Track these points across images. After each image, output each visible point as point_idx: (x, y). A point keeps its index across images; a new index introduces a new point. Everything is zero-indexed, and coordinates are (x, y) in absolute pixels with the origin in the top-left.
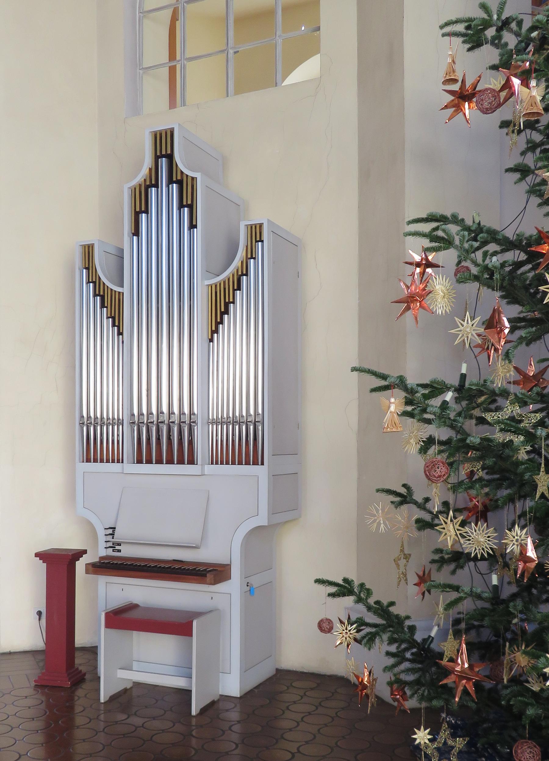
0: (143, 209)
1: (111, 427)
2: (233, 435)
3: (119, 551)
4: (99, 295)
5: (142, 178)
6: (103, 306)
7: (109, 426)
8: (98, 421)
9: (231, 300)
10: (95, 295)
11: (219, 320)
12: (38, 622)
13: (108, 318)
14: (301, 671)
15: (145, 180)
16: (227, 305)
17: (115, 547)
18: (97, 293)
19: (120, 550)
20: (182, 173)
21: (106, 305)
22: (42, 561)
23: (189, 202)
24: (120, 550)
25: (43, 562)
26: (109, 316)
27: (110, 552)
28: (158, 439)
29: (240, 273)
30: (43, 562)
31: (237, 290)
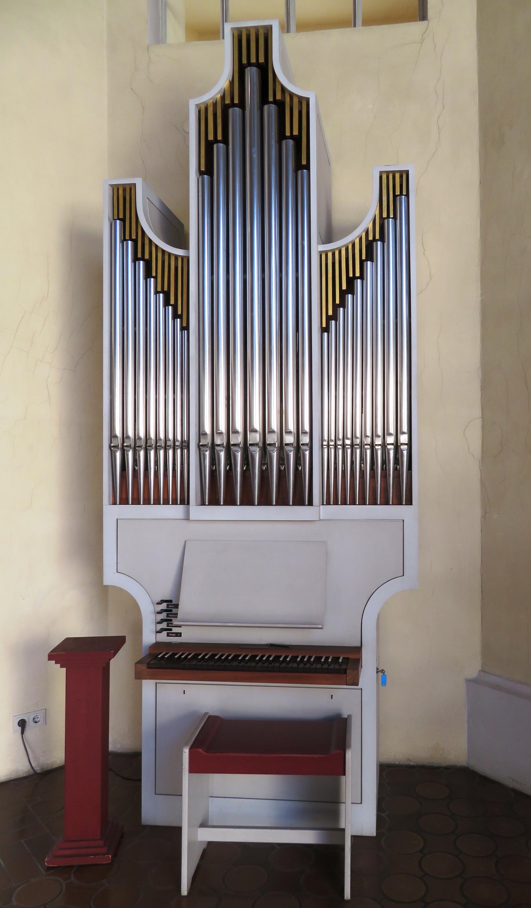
0: (220, 138)
1: (162, 452)
2: (335, 463)
3: (179, 635)
4: (143, 259)
5: (211, 99)
6: (148, 275)
7: (159, 450)
8: (151, 442)
9: (358, 274)
10: (136, 259)
11: (338, 302)
12: (21, 737)
13: (157, 292)
14: (406, 764)
15: (223, 98)
16: (351, 282)
17: (171, 630)
18: (139, 256)
19: (181, 633)
20: (284, 89)
21: (154, 274)
22: (59, 665)
23: (296, 133)
24: (181, 633)
25: (61, 667)
26: (159, 289)
27: (163, 637)
28: (336, 469)
29: (371, 238)
30: (61, 667)
31: (367, 260)
